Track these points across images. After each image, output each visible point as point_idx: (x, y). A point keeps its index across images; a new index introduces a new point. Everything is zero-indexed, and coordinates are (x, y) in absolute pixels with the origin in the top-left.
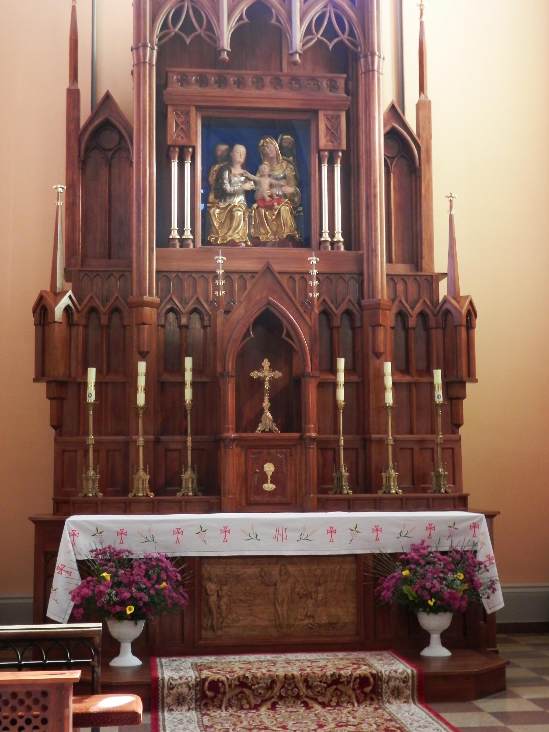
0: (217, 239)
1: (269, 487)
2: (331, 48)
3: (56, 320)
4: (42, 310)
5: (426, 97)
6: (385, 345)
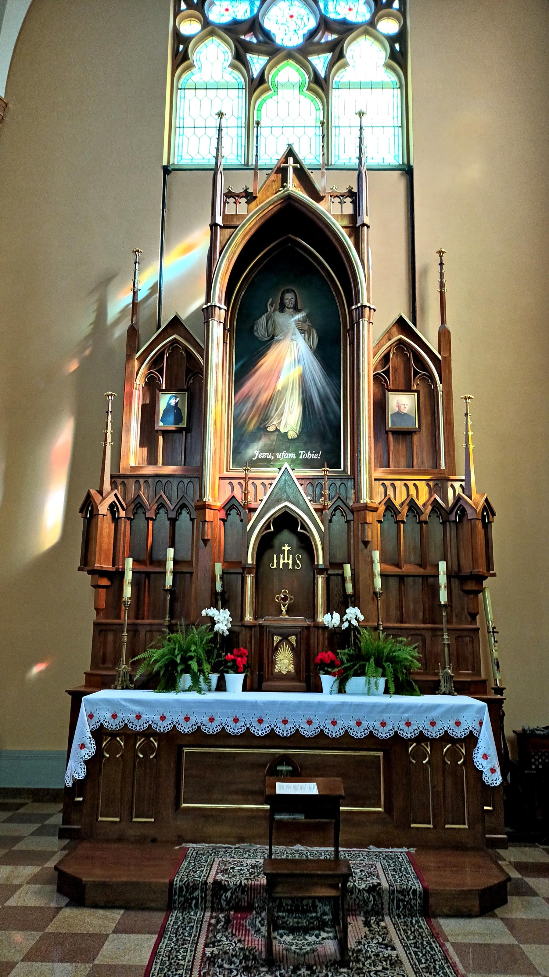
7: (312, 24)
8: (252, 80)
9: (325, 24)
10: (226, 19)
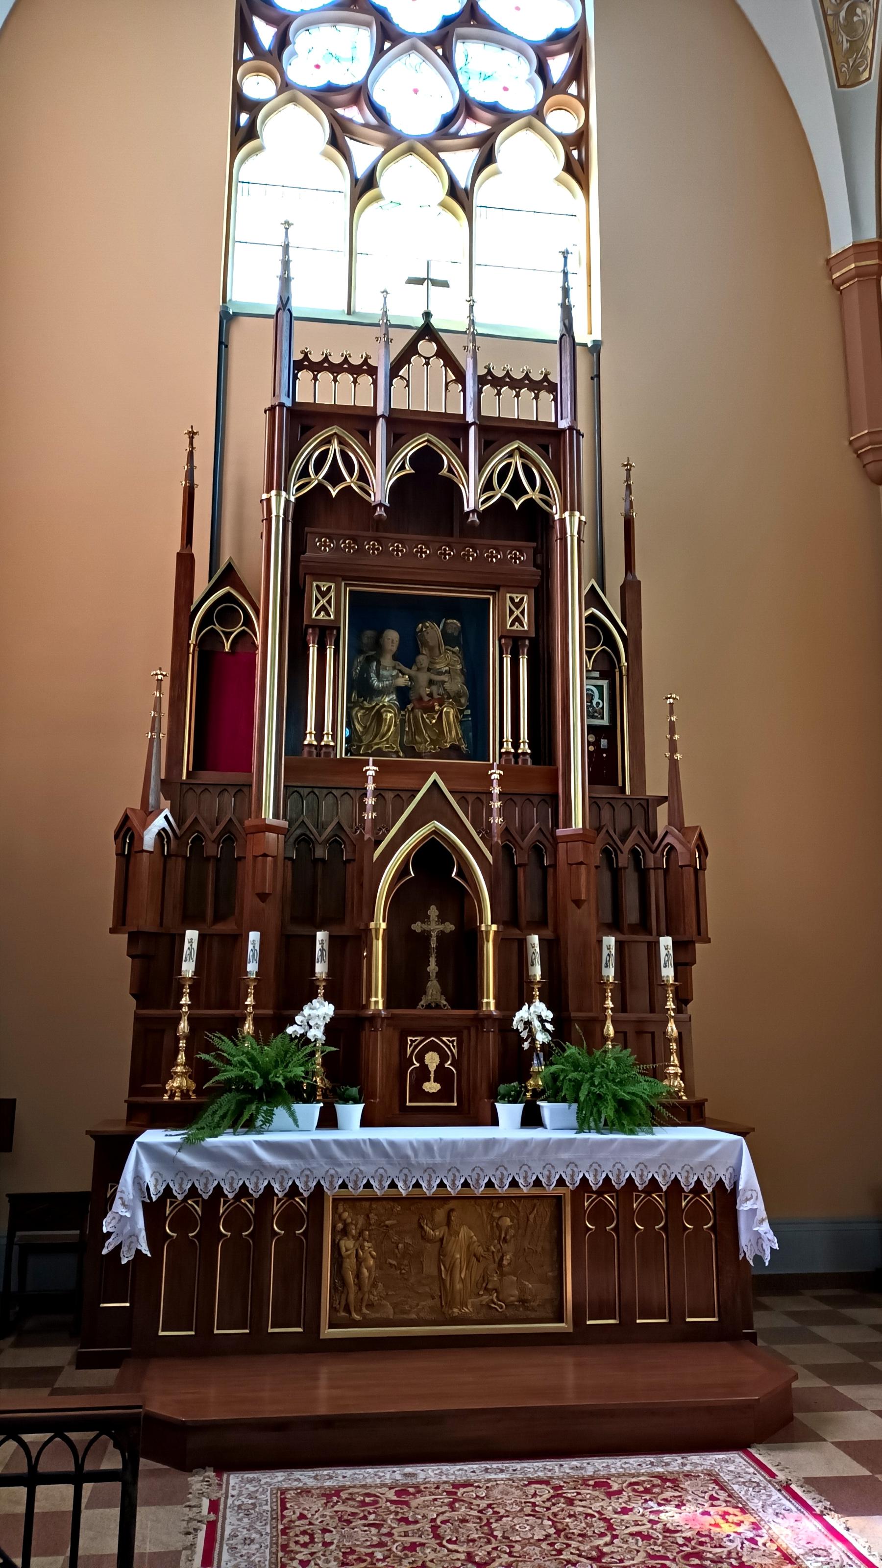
0: (359, 747)
1: (432, 1087)
2: (517, 507)
3: (145, 848)
4: (127, 832)
5: (634, 576)
6: (588, 891)
7: (449, 105)
8: (355, 181)
9: (466, 107)
10: (316, 81)
